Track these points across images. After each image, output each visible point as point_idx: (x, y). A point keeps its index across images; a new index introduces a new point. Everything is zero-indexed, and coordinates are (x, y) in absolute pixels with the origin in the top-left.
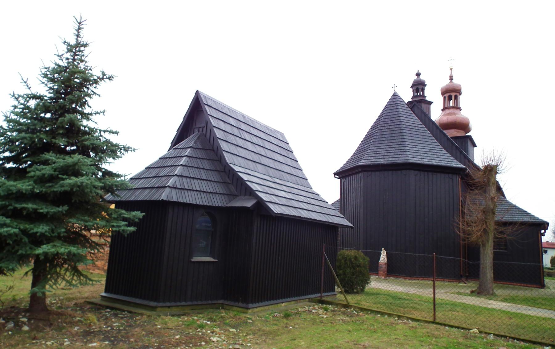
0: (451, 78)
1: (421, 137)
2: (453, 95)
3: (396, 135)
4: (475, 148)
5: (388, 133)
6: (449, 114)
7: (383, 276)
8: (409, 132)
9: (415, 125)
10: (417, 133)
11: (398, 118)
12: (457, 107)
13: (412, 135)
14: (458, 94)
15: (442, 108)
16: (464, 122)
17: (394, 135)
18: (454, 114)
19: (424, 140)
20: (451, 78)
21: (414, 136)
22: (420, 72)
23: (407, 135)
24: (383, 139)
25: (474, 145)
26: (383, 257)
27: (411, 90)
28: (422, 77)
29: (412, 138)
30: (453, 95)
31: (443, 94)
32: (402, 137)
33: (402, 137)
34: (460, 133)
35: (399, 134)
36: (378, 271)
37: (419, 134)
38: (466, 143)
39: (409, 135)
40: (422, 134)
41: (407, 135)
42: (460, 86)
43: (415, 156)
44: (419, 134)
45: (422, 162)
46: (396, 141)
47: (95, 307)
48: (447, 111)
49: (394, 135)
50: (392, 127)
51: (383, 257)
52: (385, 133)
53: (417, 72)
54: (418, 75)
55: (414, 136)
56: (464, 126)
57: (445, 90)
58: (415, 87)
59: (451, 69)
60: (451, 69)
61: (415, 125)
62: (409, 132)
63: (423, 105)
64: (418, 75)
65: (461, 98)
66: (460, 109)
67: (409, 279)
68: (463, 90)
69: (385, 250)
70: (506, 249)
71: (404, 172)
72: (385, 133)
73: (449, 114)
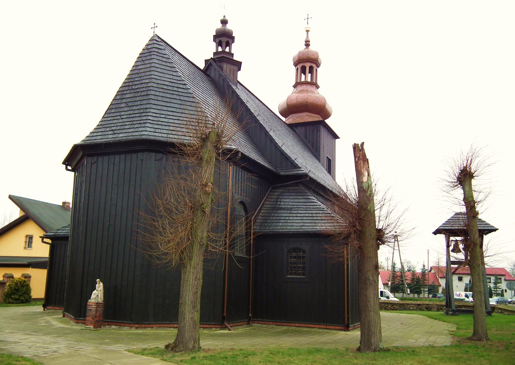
0: (307, 44)
1: (180, 102)
2: (308, 65)
3: (140, 98)
4: (337, 140)
5: (131, 95)
6: (300, 92)
7: (91, 324)
8: (161, 94)
9: (173, 85)
10: (175, 97)
11: (149, 73)
12: (314, 84)
13: (165, 99)
14: (314, 66)
15: (294, 83)
16: (319, 103)
17: (137, 99)
18: (307, 91)
19: (182, 107)
20: (307, 44)
21: (168, 100)
22: (227, 18)
23: (156, 98)
24: (123, 105)
25: (335, 137)
26: (98, 294)
27: (294, 69)
28: (229, 27)
29: (163, 104)
30: (308, 65)
31: (296, 64)
32: (148, 102)
33: (148, 102)
34: (316, 118)
35: (145, 98)
36: (85, 316)
37: (178, 97)
38: (319, 131)
39: (160, 98)
40: (182, 98)
41: (156, 98)
42: (317, 53)
43: (157, 131)
44: (178, 97)
45: (165, 139)
46: (139, 107)
47: (470, 339)
48: (300, 88)
49: (137, 99)
50: (139, 86)
51: (98, 294)
52: (127, 96)
53: (222, 18)
54: (224, 22)
55: (168, 100)
56: (321, 111)
57: (297, 59)
58: (218, 40)
59: (308, 31)
60: (308, 31)
61: (173, 85)
62: (161, 94)
63: (226, 66)
64: (224, 22)
65: (320, 71)
66: (318, 87)
67: (137, 328)
68: (322, 58)
69: (101, 281)
70: (304, 274)
71: (140, 155)
72: (127, 96)
73: (300, 92)
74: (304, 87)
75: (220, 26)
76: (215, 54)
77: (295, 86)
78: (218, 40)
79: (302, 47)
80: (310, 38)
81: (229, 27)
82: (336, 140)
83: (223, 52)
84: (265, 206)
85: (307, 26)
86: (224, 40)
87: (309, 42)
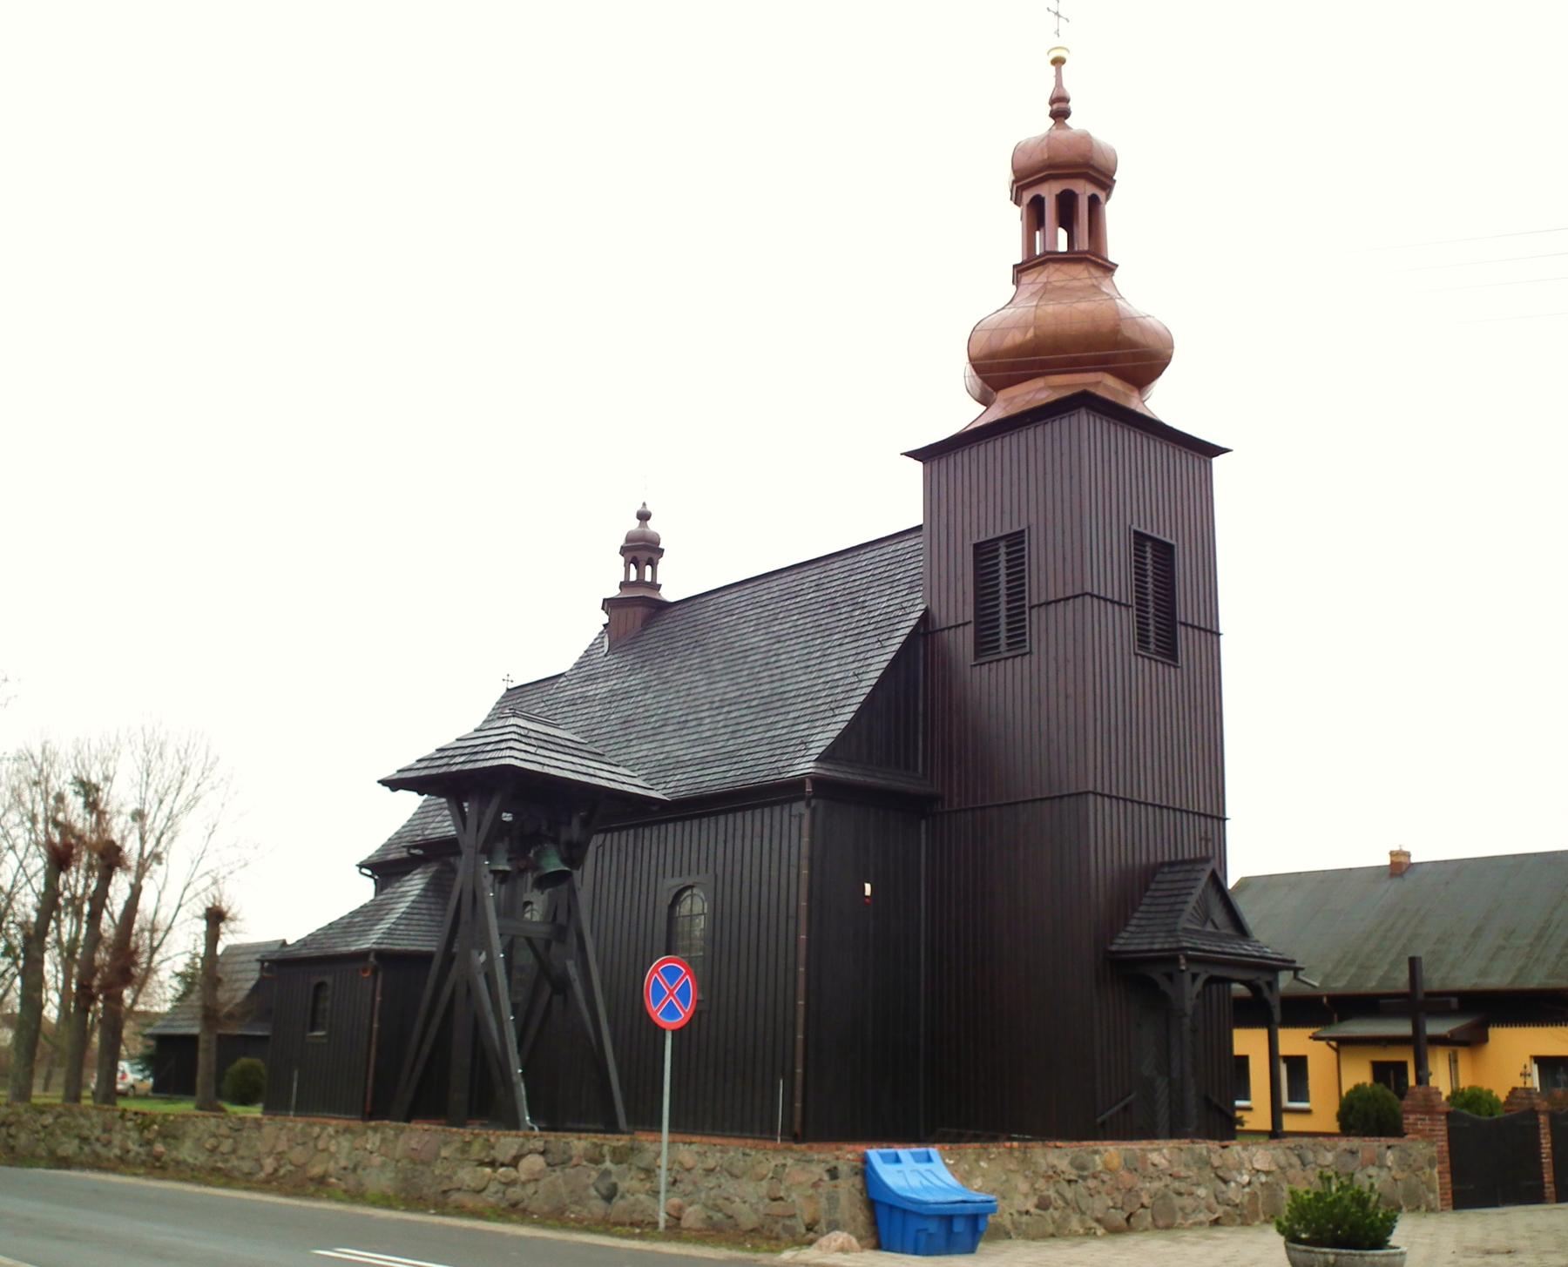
0: (1060, 111)
4: (1217, 462)
6: (1046, 292)
12: (1094, 258)
14: (1084, 190)
20: (1060, 111)
22: (649, 508)
28: (652, 525)
53: (639, 507)
54: (644, 517)
59: (1058, 62)
60: (1058, 62)
64: (644, 517)
66: (1109, 268)
74: (1055, 275)
75: (634, 524)
76: (623, 585)
77: (1020, 270)
78: (630, 555)
79: (1042, 125)
80: (1070, 88)
81: (652, 525)
82: (1215, 460)
83: (640, 582)
84: (1109, 605)
85: (1057, 42)
86: (644, 555)
87: (1065, 100)
